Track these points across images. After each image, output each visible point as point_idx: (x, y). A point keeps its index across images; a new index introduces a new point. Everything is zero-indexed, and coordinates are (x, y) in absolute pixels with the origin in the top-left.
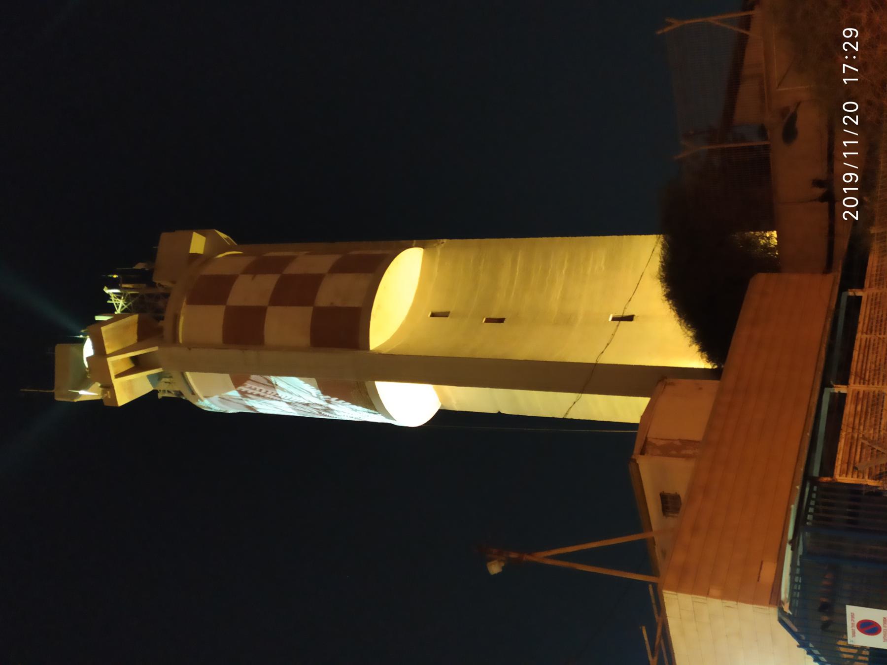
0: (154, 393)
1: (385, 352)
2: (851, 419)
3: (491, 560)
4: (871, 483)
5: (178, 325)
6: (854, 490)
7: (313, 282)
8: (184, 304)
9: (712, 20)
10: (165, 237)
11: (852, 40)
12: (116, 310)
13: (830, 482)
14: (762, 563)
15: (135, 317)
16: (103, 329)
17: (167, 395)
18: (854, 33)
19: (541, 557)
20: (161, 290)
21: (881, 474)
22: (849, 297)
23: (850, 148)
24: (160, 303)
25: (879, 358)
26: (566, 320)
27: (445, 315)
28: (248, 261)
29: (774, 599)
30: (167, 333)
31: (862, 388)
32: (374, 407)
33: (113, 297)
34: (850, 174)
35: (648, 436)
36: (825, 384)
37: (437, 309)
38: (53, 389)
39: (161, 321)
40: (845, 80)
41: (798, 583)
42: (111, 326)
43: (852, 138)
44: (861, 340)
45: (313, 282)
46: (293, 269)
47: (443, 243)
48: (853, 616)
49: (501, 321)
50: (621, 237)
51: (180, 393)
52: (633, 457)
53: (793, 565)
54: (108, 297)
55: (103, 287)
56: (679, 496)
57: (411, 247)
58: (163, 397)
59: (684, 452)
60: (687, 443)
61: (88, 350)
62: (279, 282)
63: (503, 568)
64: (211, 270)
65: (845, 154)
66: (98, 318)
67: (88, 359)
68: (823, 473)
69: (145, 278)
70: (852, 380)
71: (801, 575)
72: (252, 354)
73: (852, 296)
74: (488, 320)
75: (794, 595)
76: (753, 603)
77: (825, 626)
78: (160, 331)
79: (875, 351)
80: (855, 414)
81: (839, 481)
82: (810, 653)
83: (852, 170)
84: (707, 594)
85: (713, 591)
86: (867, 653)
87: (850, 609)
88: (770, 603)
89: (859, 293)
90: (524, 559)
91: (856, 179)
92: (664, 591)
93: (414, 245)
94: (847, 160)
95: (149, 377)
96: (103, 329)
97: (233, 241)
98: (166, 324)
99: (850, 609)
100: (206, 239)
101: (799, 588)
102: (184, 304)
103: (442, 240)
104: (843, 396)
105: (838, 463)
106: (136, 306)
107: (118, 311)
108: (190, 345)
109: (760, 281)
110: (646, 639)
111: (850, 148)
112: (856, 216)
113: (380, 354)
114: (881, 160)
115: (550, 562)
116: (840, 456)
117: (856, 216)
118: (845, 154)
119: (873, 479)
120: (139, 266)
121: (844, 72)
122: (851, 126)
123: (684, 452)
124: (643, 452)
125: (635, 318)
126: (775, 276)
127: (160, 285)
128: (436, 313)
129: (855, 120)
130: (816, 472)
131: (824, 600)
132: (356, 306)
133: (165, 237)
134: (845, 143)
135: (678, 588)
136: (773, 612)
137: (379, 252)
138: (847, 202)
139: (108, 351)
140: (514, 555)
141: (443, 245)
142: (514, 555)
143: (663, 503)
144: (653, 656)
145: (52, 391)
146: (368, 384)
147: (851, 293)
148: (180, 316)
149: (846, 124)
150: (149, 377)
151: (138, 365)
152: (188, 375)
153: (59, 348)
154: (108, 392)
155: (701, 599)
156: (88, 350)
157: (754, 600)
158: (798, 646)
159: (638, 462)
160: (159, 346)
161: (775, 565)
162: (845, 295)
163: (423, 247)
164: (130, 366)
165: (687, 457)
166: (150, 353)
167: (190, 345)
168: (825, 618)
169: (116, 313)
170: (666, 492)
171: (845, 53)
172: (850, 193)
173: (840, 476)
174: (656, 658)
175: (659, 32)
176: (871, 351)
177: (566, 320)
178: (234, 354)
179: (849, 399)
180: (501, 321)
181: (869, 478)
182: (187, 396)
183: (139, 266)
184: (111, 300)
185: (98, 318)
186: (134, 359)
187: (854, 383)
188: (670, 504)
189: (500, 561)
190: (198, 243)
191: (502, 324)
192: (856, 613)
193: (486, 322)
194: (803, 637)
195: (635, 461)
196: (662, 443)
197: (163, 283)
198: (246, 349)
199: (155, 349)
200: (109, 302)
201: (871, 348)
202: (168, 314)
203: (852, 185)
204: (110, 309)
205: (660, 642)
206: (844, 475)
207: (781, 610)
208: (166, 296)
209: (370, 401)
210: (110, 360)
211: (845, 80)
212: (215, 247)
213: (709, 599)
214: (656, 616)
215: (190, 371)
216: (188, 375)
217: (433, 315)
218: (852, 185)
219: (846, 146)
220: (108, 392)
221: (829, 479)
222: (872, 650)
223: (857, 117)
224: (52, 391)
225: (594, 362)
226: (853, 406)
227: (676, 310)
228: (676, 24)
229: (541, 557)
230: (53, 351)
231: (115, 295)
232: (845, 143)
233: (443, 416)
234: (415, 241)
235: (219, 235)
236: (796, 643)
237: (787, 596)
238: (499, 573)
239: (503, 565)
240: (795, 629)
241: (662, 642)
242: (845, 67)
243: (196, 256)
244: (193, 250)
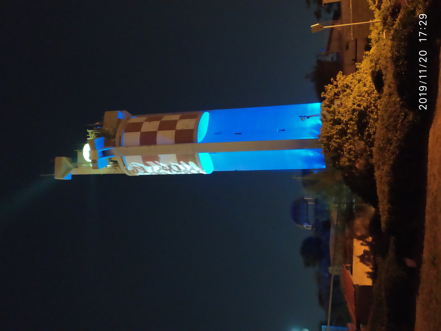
11: (424, 20)
18: (425, 88)
23: (423, 74)
34: (423, 87)
38: (54, 174)
40: (420, 40)
45: (175, 122)
65: (420, 77)
83: (424, 85)
91: (425, 17)
94: (421, 80)
98: (117, 140)
111: (423, 74)
112: (425, 108)
117: (425, 60)
118: (420, 77)
121: (420, 36)
122: (423, 63)
129: (425, 107)
132: (192, 129)
134: (420, 71)
149: (421, 62)
171: (420, 27)
172: (423, 96)
184: (89, 135)
203: (424, 92)
211: (420, 40)
218: (424, 92)
223: (426, 58)
232: (420, 71)
242: (420, 33)
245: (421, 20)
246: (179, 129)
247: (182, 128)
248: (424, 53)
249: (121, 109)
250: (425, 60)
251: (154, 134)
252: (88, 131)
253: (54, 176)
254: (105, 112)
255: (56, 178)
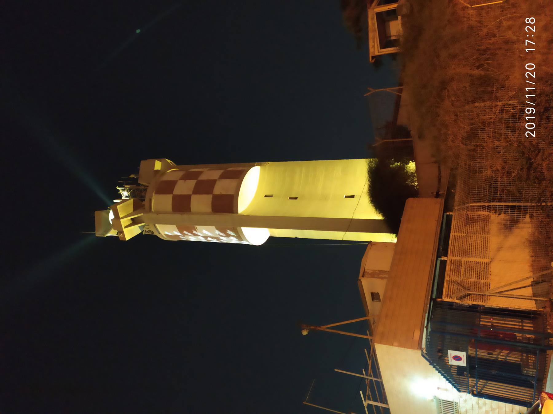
0: (142, 233)
1: (245, 214)
2: (449, 273)
3: (304, 329)
4: (457, 301)
5: (152, 204)
6: (450, 304)
7: (212, 183)
8: (154, 194)
9: (388, 90)
10: (143, 163)
12: (122, 197)
13: (441, 301)
14: (414, 331)
15: (132, 200)
16: (118, 207)
17: (147, 233)
19: (323, 328)
20: (143, 187)
21: (461, 297)
22: (447, 215)
23: (530, 92)
24: (143, 194)
25: (459, 244)
26: (325, 198)
27: (271, 196)
28: (181, 174)
29: (420, 347)
30: (147, 206)
31: (453, 258)
32: (242, 239)
33: (121, 191)
34: (530, 109)
35: (365, 269)
36: (438, 256)
37: (267, 194)
38: (95, 231)
39: (144, 202)
41: (429, 339)
42: (121, 205)
43: (530, 86)
44: (452, 235)
45: (212, 183)
46: (203, 177)
47: (269, 163)
48: (451, 354)
49: (296, 198)
50: (348, 160)
51: (153, 233)
52: (359, 278)
53: (427, 335)
54: (119, 191)
55: (116, 187)
56: (379, 294)
57: (254, 166)
58: (145, 234)
59: (381, 276)
60: (382, 272)
61: (111, 216)
62: (196, 184)
63: (308, 332)
64: (165, 178)
65: (527, 96)
66: (115, 201)
67: (112, 220)
68: (437, 297)
69: (134, 182)
70: (449, 255)
71: (429, 336)
72: (185, 216)
73: (448, 215)
74: (290, 198)
75: (428, 340)
76: (411, 349)
77: (440, 357)
78: (143, 206)
79: (458, 241)
80: (450, 270)
81: (444, 300)
82: (434, 367)
83: (531, 106)
84: (392, 345)
85: (395, 344)
86: (457, 367)
87: (450, 352)
88: (418, 349)
89: (451, 213)
90: (317, 329)
92: (375, 344)
93: (256, 165)
95: (139, 227)
96: (118, 207)
97: (174, 164)
98: (146, 203)
99: (450, 352)
100: (162, 163)
101: (429, 341)
102: (154, 194)
103: (268, 162)
104: (445, 262)
105: (444, 294)
106: (132, 195)
107: (123, 198)
108: (157, 213)
109: (410, 202)
110: (367, 354)
113: (243, 215)
114: (458, 182)
115: (327, 330)
116: (444, 290)
118: (527, 96)
119: (458, 300)
120: (131, 176)
122: (530, 78)
123: (381, 276)
124: (363, 276)
125: (355, 196)
126: (416, 199)
127: (142, 185)
128: (267, 195)
129: (533, 75)
130: (434, 297)
131: (439, 348)
132: (232, 194)
133: (143, 163)
134: (527, 89)
135: (380, 342)
136: (419, 352)
137: (241, 169)
138: (528, 126)
139: (121, 216)
140: (313, 328)
141: (269, 164)
142: (313, 328)
143: (372, 295)
144: (370, 360)
145: (94, 232)
146: (238, 228)
147: (448, 214)
148: (152, 199)
150: (139, 227)
151: (134, 222)
152: (157, 225)
153: (97, 213)
154: (121, 234)
155: (391, 347)
156: (111, 216)
157: (412, 347)
158: (429, 365)
159: (361, 280)
160: (143, 213)
161: (420, 331)
162: (445, 214)
163: (260, 166)
164: (131, 222)
165: (382, 278)
166: (139, 216)
167: (157, 213)
168: (440, 354)
169: (123, 198)
170: (373, 292)
171: (527, 33)
172: (530, 120)
173: (445, 298)
174: (371, 361)
175: (365, 95)
176: (456, 241)
177: (325, 198)
178: (178, 216)
179: (448, 263)
180: (296, 198)
181: (456, 299)
182: (156, 234)
183: (131, 176)
184: (120, 192)
185: (115, 201)
186: (132, 219)
187: (450, 256)
188: (375, 296)
189: (307, 330)
190: (158, 165)
191: (296, 200)
192: (452, 353)
193: (289, 199)
194: (432, 362)
195: (360, 280)
196: (371, 272)
197: (143, 184)
198: (183, 214)
199: (142, 214)
200: (119, 193)
201: (456, 240)
202: (147, 199)
203: (532, 115)
204: (120, 197)
205: (372, 354)
206: (446, 298)
207: (422, 351)
208: (145, 190)
209: (239, 236)
210: (122, 220)
212: (166, 167)
213: (393, 347)
214: (370, 343)
215: (158, 224)
216: (157, 225)
217: (266, 196)
218: (532, 115)
219: (527, 91)
220: (121, 234)
221: (440, 299)
222: (458, 366)
224: (94, 232)
225: (342, 240)
226: (449, 266)
227: (371, 181)
228: (372, 91)
229: (323, 328)
230: (94, 214)
231: (122, 190)
232: (527, 89)
233: (271, 239)
234: (256, 163)
235: (167, 161)
236: (428, 363)
237: (425, 347)
238: (306, 335)
239: (308, 331)
240: (429, 359)
241: (373, 353)
243: (158, 171)
244: (156, 168)
245: (529, 25)
246: (217, 194)
247: (221, 193)
248: (532, 66)
249: (159, 157)
250: (533, 29)
251: (188, 198)
252: (118, 188)
253: (95, 233)
254: (141, 161)
255: (97, 235)
